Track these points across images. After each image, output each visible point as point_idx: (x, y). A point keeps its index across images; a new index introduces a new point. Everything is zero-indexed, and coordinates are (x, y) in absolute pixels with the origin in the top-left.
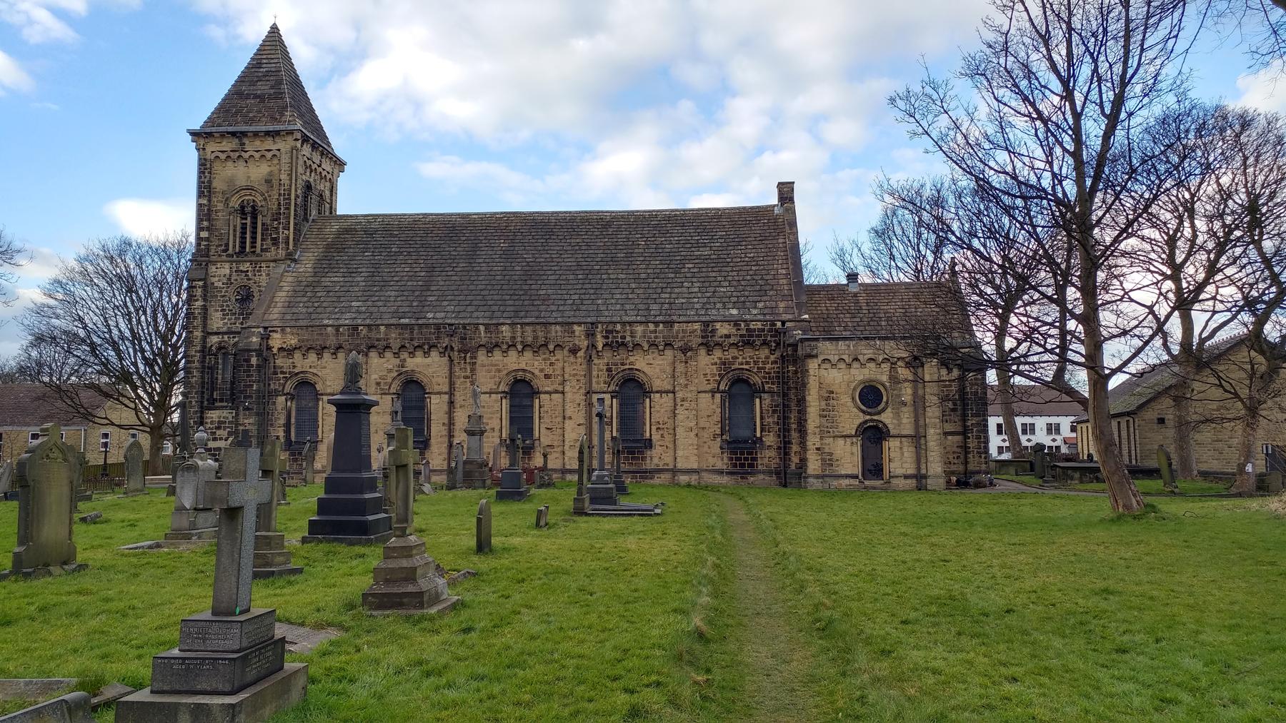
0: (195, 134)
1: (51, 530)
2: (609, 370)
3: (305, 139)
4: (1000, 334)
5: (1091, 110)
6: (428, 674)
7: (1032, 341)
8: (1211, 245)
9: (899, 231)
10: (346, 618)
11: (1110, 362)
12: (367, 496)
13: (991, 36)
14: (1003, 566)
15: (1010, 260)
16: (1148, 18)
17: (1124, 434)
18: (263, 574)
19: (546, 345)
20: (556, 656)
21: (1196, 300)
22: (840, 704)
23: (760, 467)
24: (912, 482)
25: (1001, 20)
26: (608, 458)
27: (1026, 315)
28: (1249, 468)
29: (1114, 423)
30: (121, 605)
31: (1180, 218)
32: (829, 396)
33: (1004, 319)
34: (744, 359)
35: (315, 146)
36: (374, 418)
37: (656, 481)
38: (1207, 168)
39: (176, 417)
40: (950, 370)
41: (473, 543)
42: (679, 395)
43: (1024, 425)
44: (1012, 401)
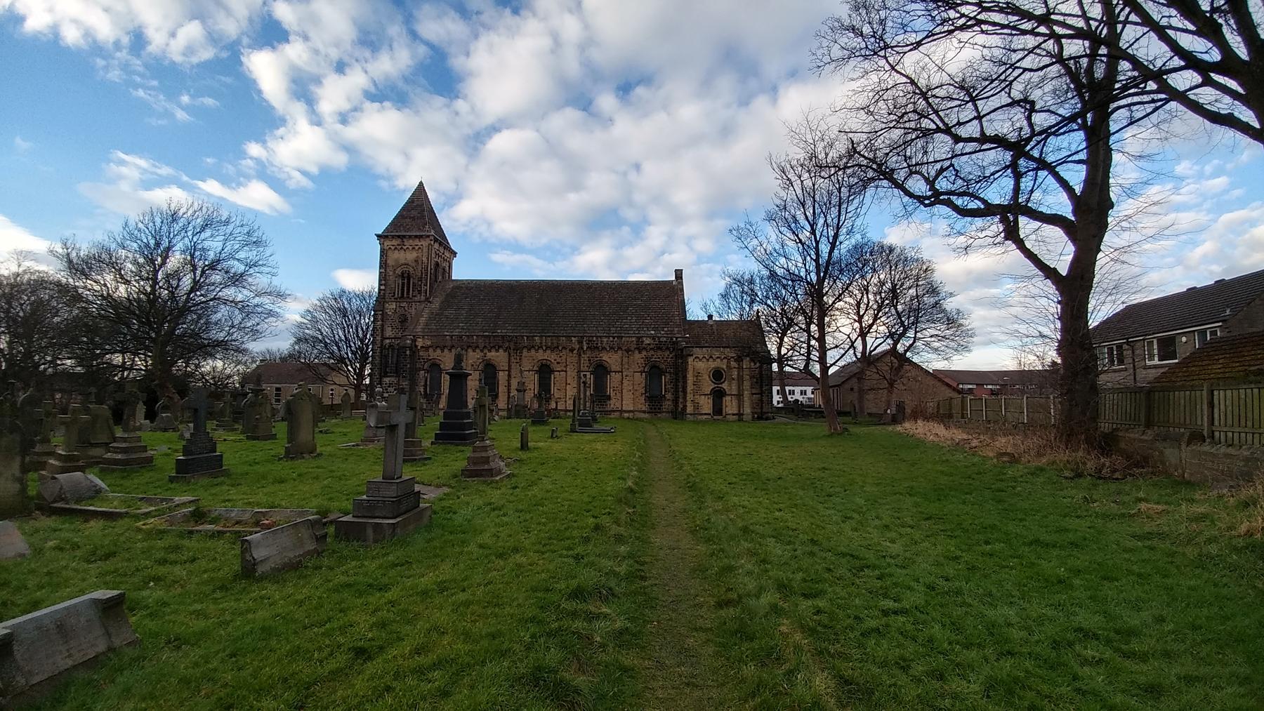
0: (379, 236)
1: (304, 436)
2: (589, 360)
3: (436, 240)
4: (779, 349)
5: (824, 240)
6: (494, 510)
7: (794, 350)
8: (875, 307)
9: (732, 295)
10: (453, 482)
11: (830, 361)
12: (465, 421)
13: (778, 202)
14: (778, 457)
15: (785, 311)
16: (849, 196)
17: (835, 395)
18: (410, 459)
19: (558, 347)
20: (559, 500)
21: (868, 332)
22: (698, 522)
24: (736, 417)
25: (783, 194)
26: (588, 404)
27: (792, 337)
28: (889, 411)
29: (831, 390)
30: (339, 474)
31: (862, 293)
32: (698, 375)
33: (782, 339)
34: (657, 357)
35: (441, 244)
36: (469, 383)
37: (612, 416)
38: (874, 270)
39: (367, 381)
40: (755, 364)
41: (519, 445)
42: (625, 374)
43: (790, 391)
44: (784, 379)
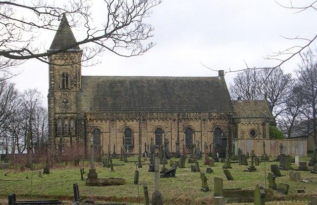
2: (183, 126)
23: (5, 153)
42: (203, 133)
